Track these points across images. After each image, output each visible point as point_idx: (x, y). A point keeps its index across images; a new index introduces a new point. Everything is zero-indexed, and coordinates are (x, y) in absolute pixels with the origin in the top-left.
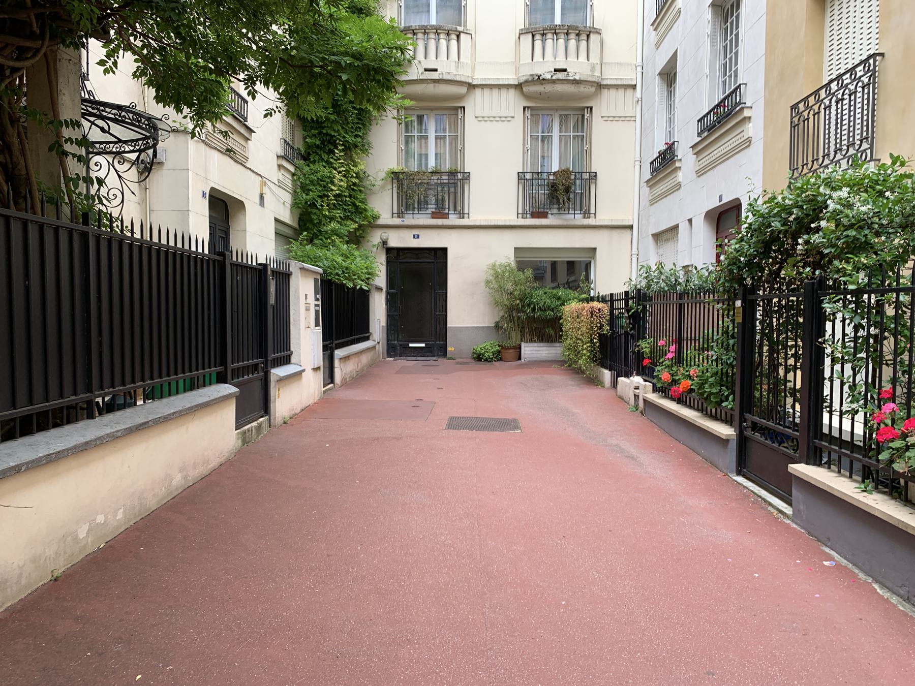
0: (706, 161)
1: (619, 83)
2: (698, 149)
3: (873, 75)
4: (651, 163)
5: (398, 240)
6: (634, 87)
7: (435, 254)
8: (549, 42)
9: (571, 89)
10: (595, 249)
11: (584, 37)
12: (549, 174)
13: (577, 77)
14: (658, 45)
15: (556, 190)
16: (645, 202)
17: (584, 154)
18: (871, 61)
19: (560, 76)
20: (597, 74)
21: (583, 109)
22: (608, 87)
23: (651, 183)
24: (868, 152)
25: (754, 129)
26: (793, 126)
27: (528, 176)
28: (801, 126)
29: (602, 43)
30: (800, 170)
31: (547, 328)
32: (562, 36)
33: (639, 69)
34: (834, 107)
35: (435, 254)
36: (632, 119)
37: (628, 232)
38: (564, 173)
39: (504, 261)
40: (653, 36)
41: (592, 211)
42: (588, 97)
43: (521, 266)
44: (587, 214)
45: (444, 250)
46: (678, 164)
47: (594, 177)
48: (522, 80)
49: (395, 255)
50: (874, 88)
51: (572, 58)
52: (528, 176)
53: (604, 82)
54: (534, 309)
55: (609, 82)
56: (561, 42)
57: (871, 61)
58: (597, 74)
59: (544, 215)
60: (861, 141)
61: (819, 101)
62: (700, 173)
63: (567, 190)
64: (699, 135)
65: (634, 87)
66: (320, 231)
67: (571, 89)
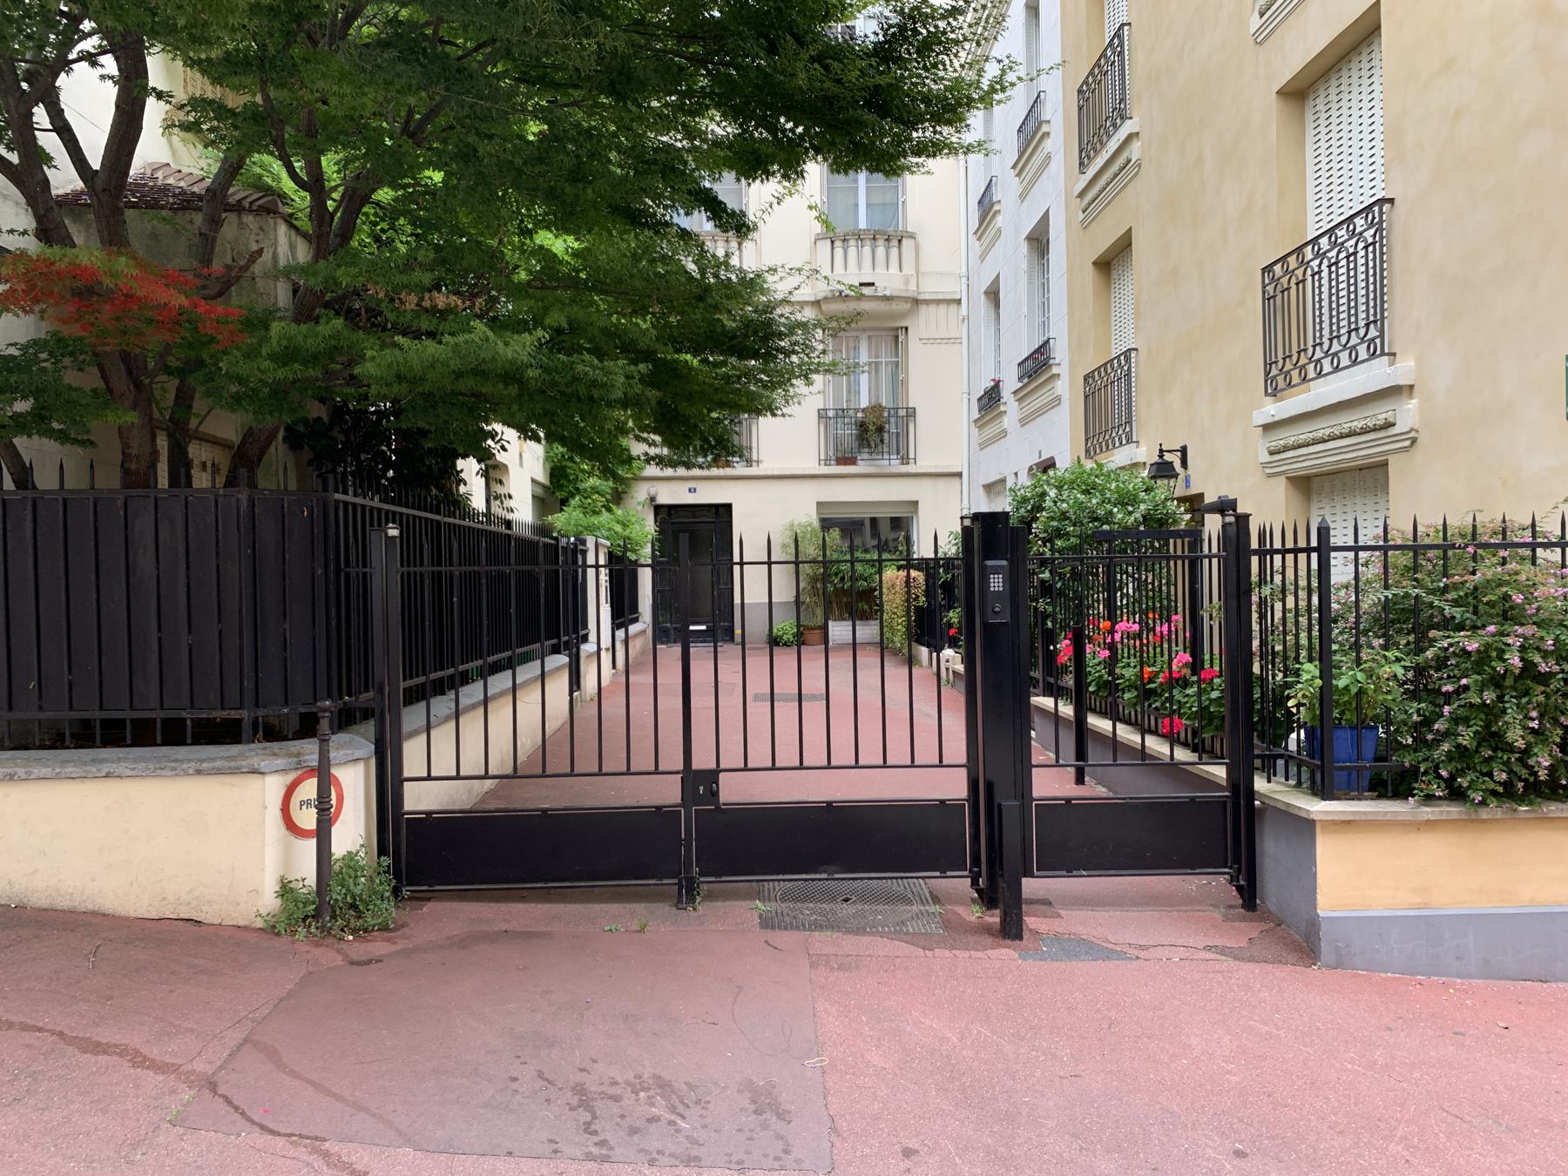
0: (1027, 411)
1: (940, 297)
2: (1021, 395)
3: (1380, 230)
4: (979, 400)
5: (672, 494)
6: (959, 302)
7: (717, 513)
8: (852, 251)
9: (882, 307)
10: (916, 503)
11: (895, 243)
12: (857, 410)
13: (888, 293)
14: (982, 258)
15: (866, 431)
16: (975, 445)
17: (898, 384)
18: (1376, 209)
19: (867, 291)
20: (913, 287)
21: (897, 329)
22: (927, 302)
23: (980, 423)
24: (1378, 341)
25: (1062, 387)
26: (1268, 299)
27: (831, 414)
28: (1279, 299)
29: (917, 248)
30: (1280, 364)
31: (858, 601)
32: (868, 243)
33: (964, 280)
34: (1325, 274)
35: (717, 513)
36: (957, 340)
37: (956, 481)
38: (876, 409)
39: (803, 520)
40: (976, 247)
41: (912, 455)
42: (903, 315)
43: (826, 524)
44: (905, 460)
45: (728, 507)
46: (1002, 408)
47: (911, 413)
48: (820, 296)
49: (665, 514)
50: (1382, 246)
51: (881, 269)
52: (831, 414)
53: (921, 297)
54: (843, 579)
55: (927, 297)
56: (867, 249)
57: (1376, 209)
58: (913, 287)
59: (852, 461)
60: (1367, 325)
61: (1304, 264)
62: (1024, 422)
63: (880, 430)
64: (1020, 379)
65: (959, 302)
66: (577, 489)
67: (882, 307)
